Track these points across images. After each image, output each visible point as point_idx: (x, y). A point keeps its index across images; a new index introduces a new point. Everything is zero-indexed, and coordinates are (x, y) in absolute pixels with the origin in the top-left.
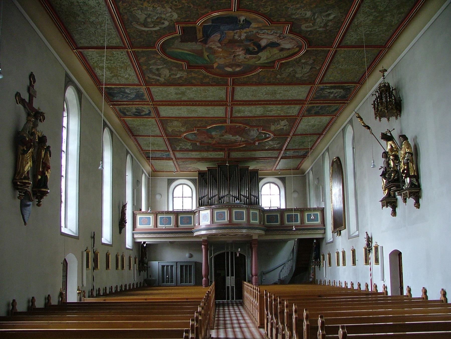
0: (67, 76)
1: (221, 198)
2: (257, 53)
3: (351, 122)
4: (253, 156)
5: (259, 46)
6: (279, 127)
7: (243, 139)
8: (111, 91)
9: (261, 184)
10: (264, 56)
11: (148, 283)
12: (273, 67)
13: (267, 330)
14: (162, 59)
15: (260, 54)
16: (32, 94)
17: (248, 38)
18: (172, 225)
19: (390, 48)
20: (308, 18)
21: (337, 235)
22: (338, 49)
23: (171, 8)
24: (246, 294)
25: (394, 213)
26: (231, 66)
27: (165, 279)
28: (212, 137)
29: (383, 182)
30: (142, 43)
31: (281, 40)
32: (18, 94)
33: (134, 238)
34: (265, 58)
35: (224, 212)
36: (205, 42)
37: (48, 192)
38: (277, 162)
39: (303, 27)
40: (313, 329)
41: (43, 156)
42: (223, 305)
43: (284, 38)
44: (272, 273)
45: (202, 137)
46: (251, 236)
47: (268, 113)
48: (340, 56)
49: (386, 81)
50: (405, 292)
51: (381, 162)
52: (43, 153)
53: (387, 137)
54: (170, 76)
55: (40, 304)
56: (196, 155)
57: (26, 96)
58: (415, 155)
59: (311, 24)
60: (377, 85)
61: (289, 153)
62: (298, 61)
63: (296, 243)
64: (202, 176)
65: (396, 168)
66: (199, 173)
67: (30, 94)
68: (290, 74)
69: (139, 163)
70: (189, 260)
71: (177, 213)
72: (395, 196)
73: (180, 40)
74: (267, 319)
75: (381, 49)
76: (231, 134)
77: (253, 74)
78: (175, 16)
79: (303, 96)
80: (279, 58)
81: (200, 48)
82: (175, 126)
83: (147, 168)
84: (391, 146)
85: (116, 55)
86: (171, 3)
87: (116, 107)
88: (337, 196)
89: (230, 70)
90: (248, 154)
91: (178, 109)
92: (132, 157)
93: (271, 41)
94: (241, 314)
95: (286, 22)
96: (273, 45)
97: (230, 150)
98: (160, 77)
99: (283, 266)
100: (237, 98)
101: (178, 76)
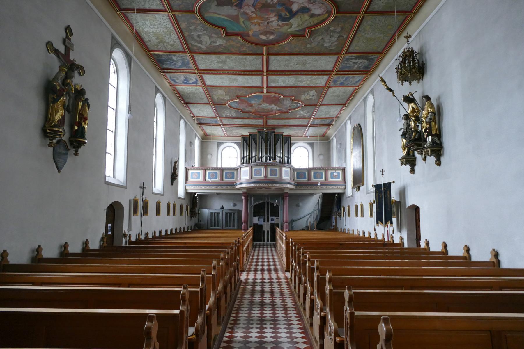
0: (113, 38)
2: (289, 19)
3: (372, 92)
4: (287, 124)
5: (290, 11)
6: (308, 97)
7: (278, 108)
9: (293, 148)
10: (296, 24)
11: (198, 227)
12: (303, 36)
15: (291, 21)
16: (69, 46)
18: (218, 179)
19: (415, 14)
24: (278, 238)
25: (413, 171)
26: (265, 33)
27: (214, 223)
28: (251, 106)
29: (401, 142)
30: (181, 6)
32: (49, 44)
33: (186, 189)
34: (296, 25)
35: (261, 169)
37: (85, 143)
41: (80, 107)
46: (284, 190)
49: (410, 46)
50: (423, 245)
51: (402, 124)
52: (81, 104)
53: (409, 99)
54: (211, 43)
55: (75, 248)
56: (239, 122)
57: (62, 49)
58: (437, 114)
60: (402, 51)
61: (317, 122)
65: (416, 128)
67: (66, 46)
68: (319, 43)
70: (233, 208)
71: (222, 170)
72: (414, 155)
74: (292, 266)
75: (407, 14)
76: (267, 103)
77: (286, 42)
79: (330, 67)
80: (309, 25)
82: (219, 95)
83: (198, 132)
84: (413, 108)
87: (167, 74)
89: (264, 38)
93: (302, 5)
97: (267, 119)
98: (202, 44)
101: (218, 44)
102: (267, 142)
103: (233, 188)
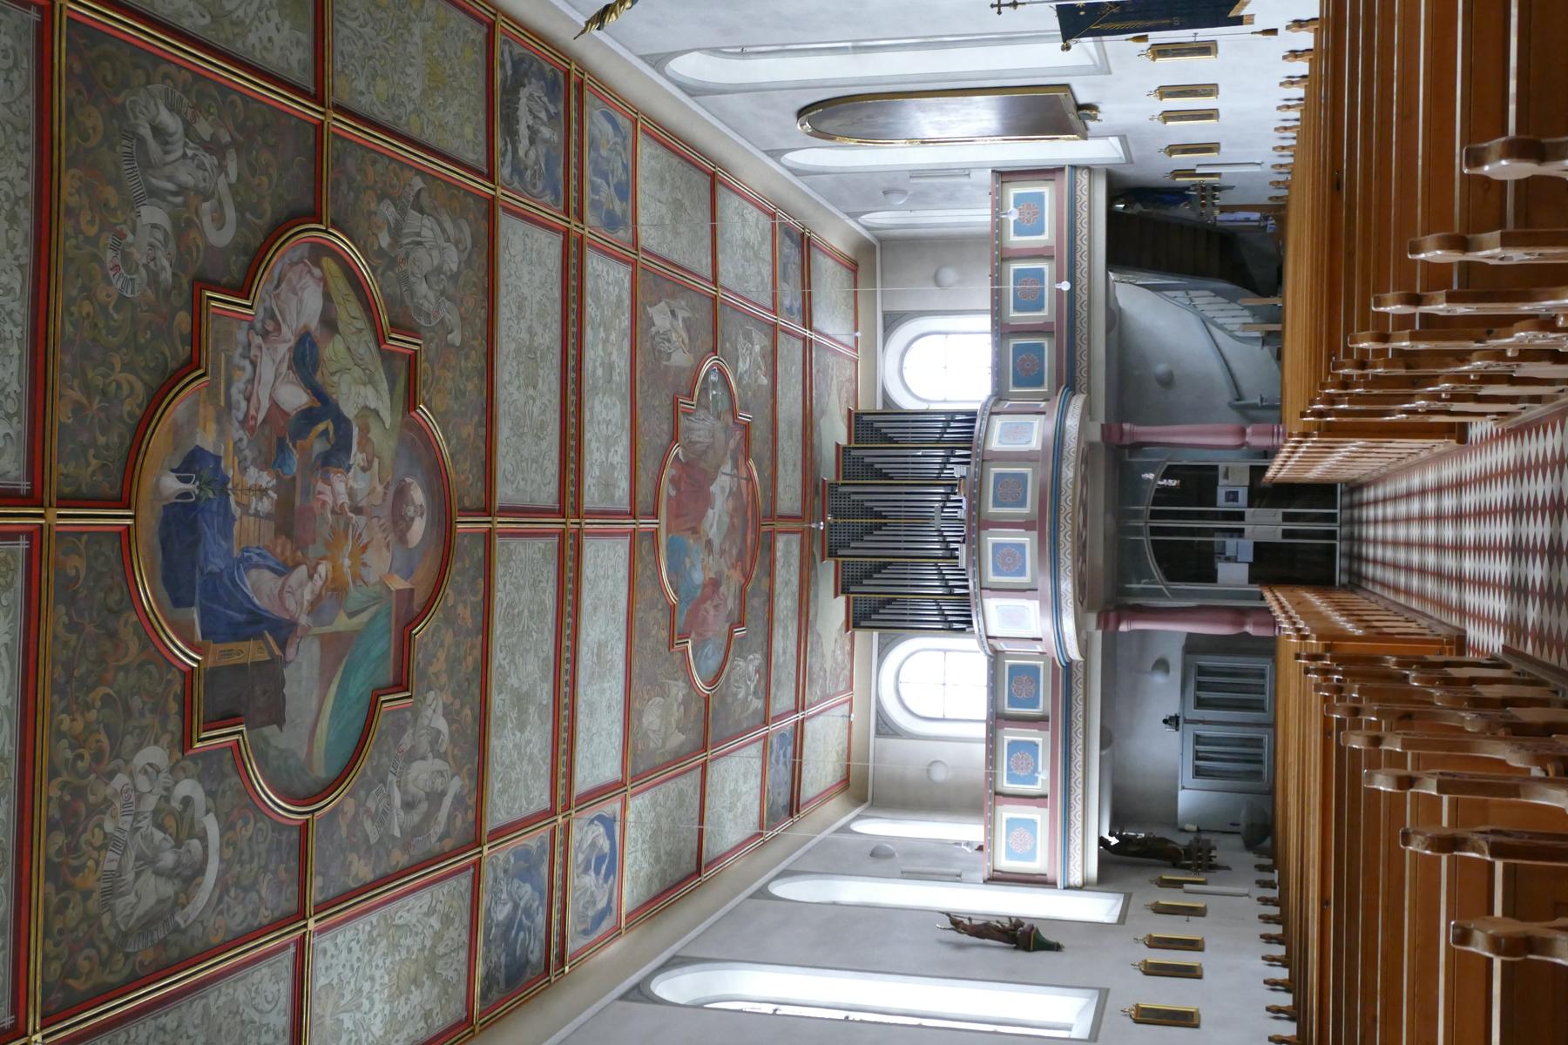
1: (947, 549)
2: (341, 422)
3: (657, 62)
4: (798, 430)
5: (308, 417)
6: (679, 335)
7: (727, 468)
8: (501, 976)
9: (907, 403)
10: (363, 394)
11: (1262, 835)
13: (1484, 414)
14: (362, 793)
15: (349, 411)
17: (274, 458)
18: (1039, 738)
20: (175, 221)
21: (1094, 118)
22: (330, 99)
23: (111, 775)
24: (1315, 473)
26: (399, 523)
27: (1245, 764)
28: (715, 584)
30: (283, 875)
31: (284, 328)
33: (1084, 886)
34: (369, 391)
35: (996, 546)
36: (284, 630)
38: (826, 342)
39: (222, 237)
40: (1537, 210)
42: (1356, 558)
43: (273, 317)
44: (1235, 365)
45: (710, 618)
46: (1092, 446)
47: (616, 378)
48: (362, 93)
56: (785, 637)
59: (206, 206)
62: (386, 261)
63: (1125, 277)
64: (867, 617)
66: (857, 626)
69: (809, 845)
71: (997, 719)
73: (270, 731)
76: (701, 516)
78: (154, 754)
80: (368, 336)
81: (315, 648)
82: (663, 722)
85: (334, 974)
86: (84, 776)
87: (571, 947)
88: (945, 119)
89: (418, 529)
90: (789, 449)
91: (591, 714)
92: (786, 874)
93: (285, 366)
94: (1396, 498)
95: (196, 308)
96: (305, 360)
97: (773, 516)
98: (443, 794)
99: (1214, 330)
100: (547, 495)
101: (441, 724)
102: (879, 515)
103: (1078, 674)
